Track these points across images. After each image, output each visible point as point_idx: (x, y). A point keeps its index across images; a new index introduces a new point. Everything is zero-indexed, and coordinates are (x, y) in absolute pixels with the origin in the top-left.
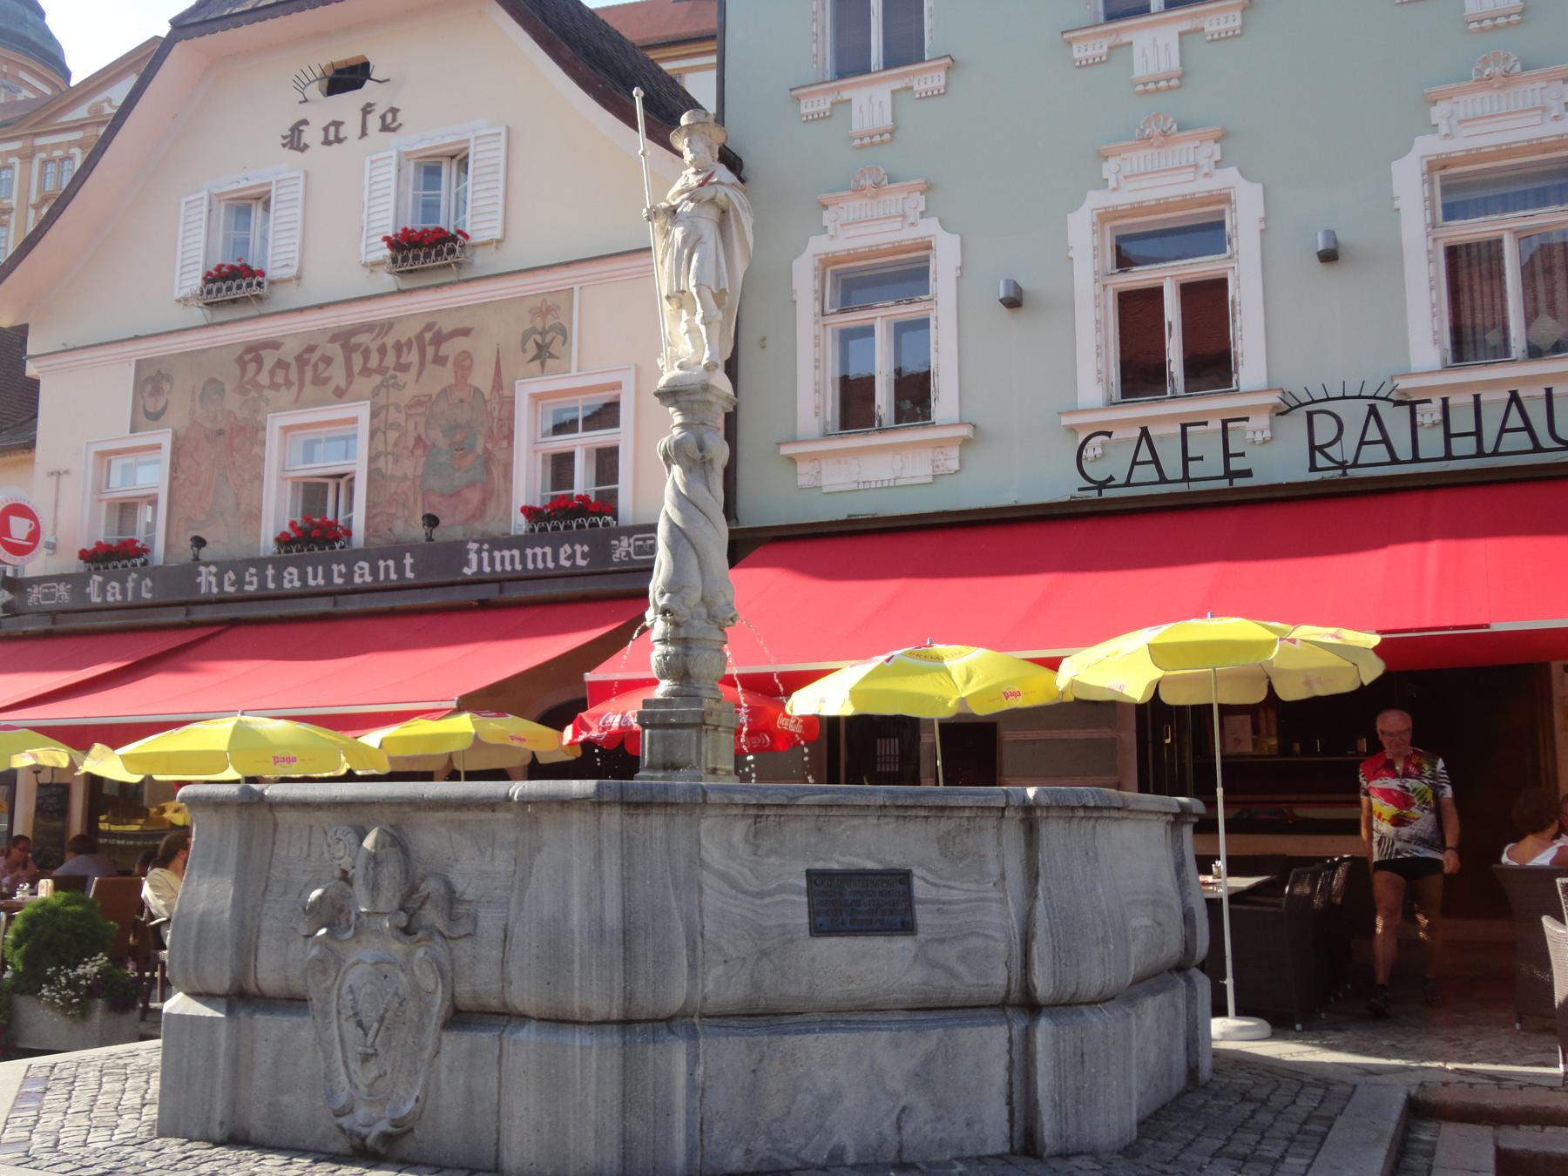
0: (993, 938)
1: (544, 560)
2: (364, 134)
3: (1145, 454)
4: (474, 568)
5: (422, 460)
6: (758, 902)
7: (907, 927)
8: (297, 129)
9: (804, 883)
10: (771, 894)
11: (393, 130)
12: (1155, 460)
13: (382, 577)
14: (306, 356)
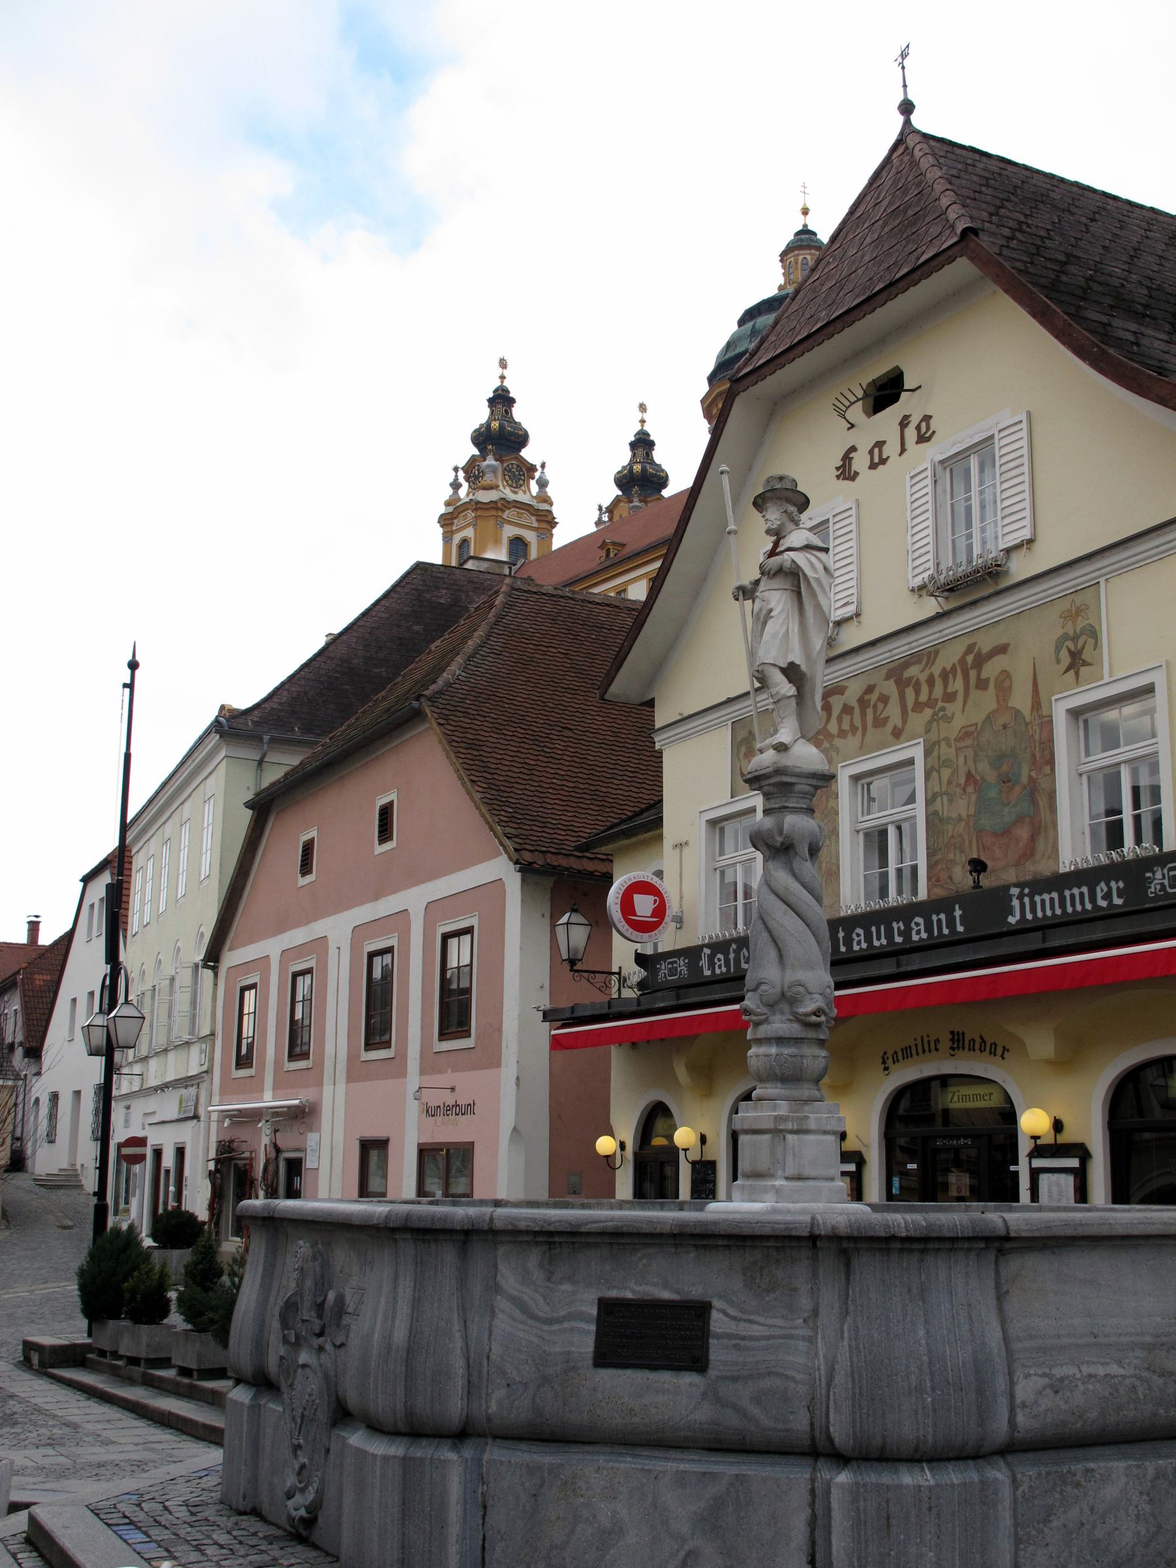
0: (793, 1379)
1: (1082, 903)
2: (903, 450)
4: (1018, 917)
5: (974, 797)
6: (546, 1328)
7: (698, 1363)
8: (847, 458)
9: (595, 1312)
10: (559, 1321)
11: (928, 439)
14: (867, 697)
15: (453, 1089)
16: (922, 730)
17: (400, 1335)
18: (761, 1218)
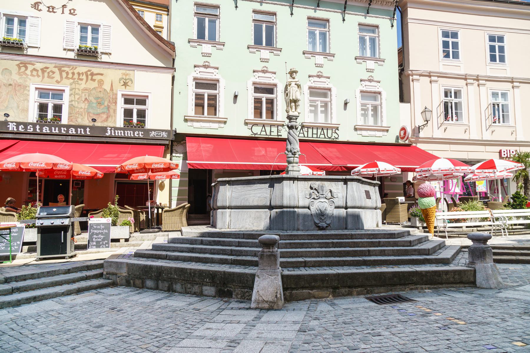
4: (109, 134)
5: (87, 104)
12: (265, 131)
13: (79, 133)
18: (164, 245)
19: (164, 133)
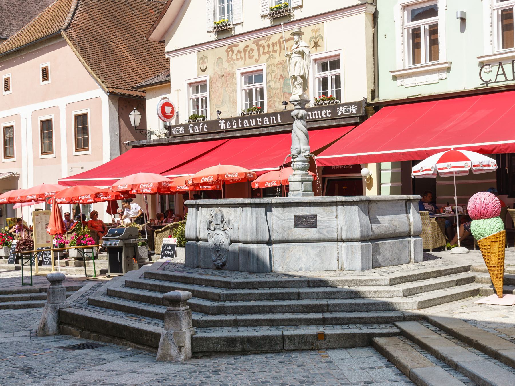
1: (318, 115)
3: (501, 72)
5: (282, 82)
7: (316, 226)
12: (504, 74)
14: (246, 49)
15: (82, 168)
16: (265, 61)
17: (254, 224)
19: (353, 107)
